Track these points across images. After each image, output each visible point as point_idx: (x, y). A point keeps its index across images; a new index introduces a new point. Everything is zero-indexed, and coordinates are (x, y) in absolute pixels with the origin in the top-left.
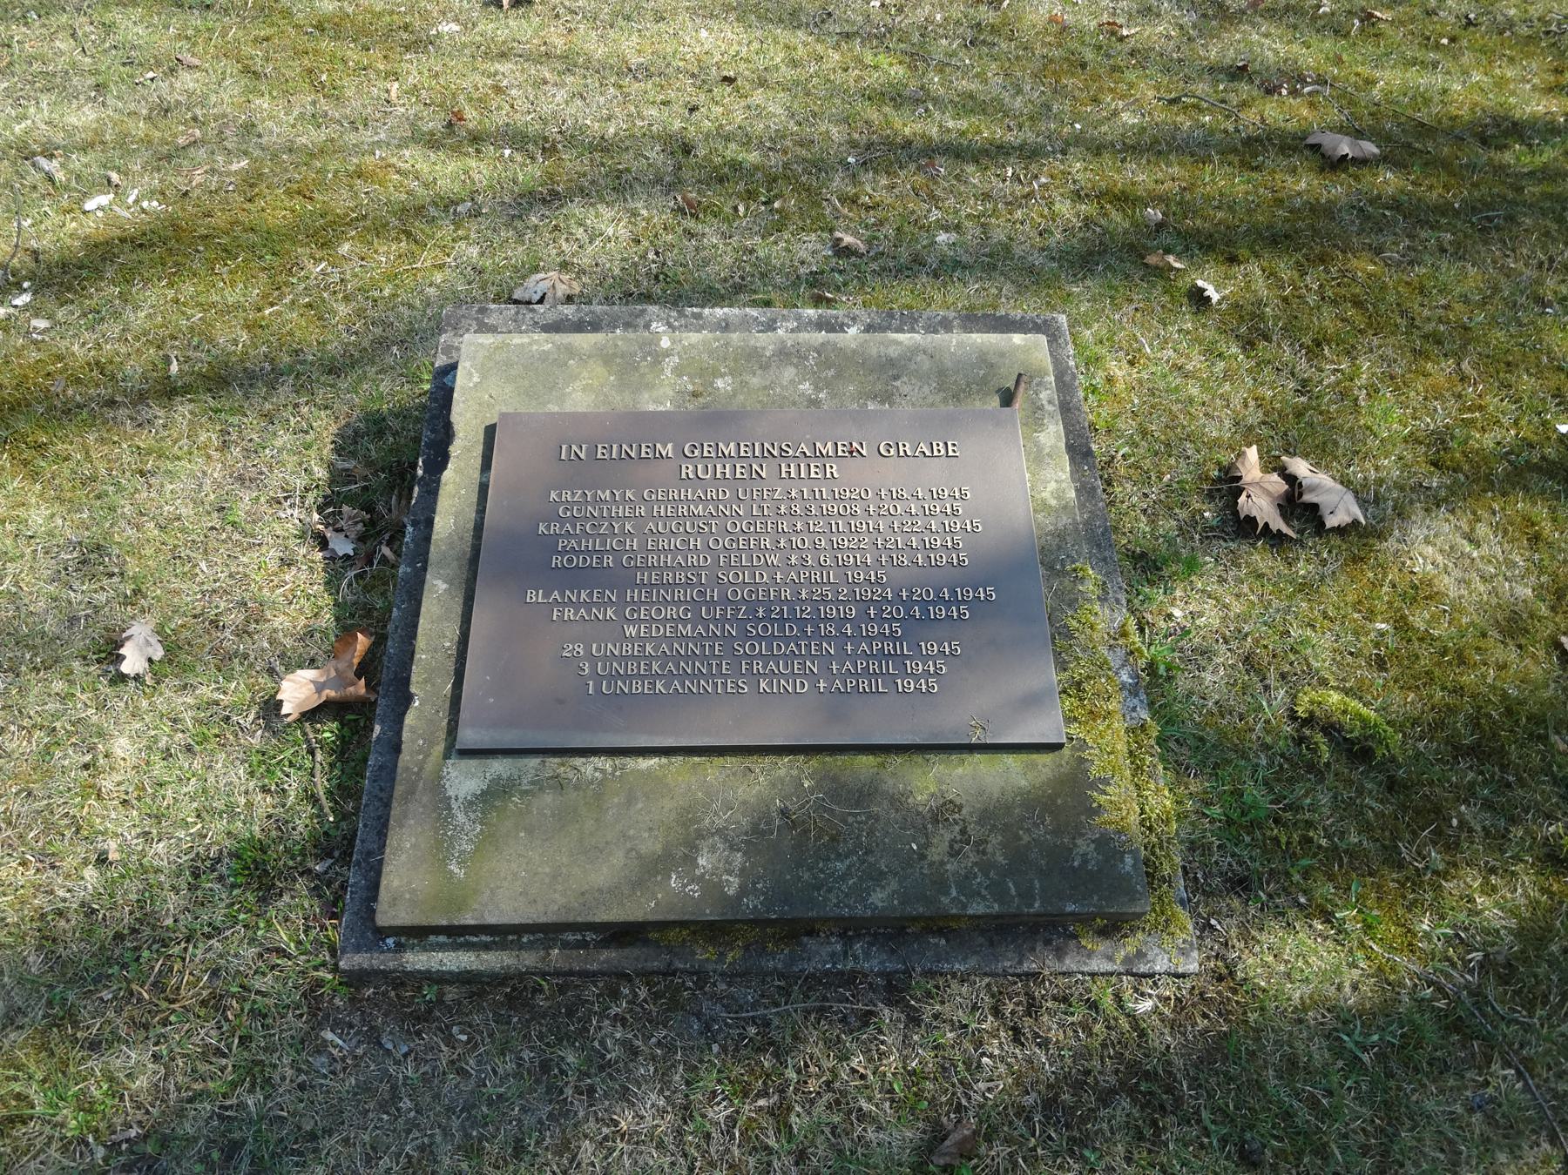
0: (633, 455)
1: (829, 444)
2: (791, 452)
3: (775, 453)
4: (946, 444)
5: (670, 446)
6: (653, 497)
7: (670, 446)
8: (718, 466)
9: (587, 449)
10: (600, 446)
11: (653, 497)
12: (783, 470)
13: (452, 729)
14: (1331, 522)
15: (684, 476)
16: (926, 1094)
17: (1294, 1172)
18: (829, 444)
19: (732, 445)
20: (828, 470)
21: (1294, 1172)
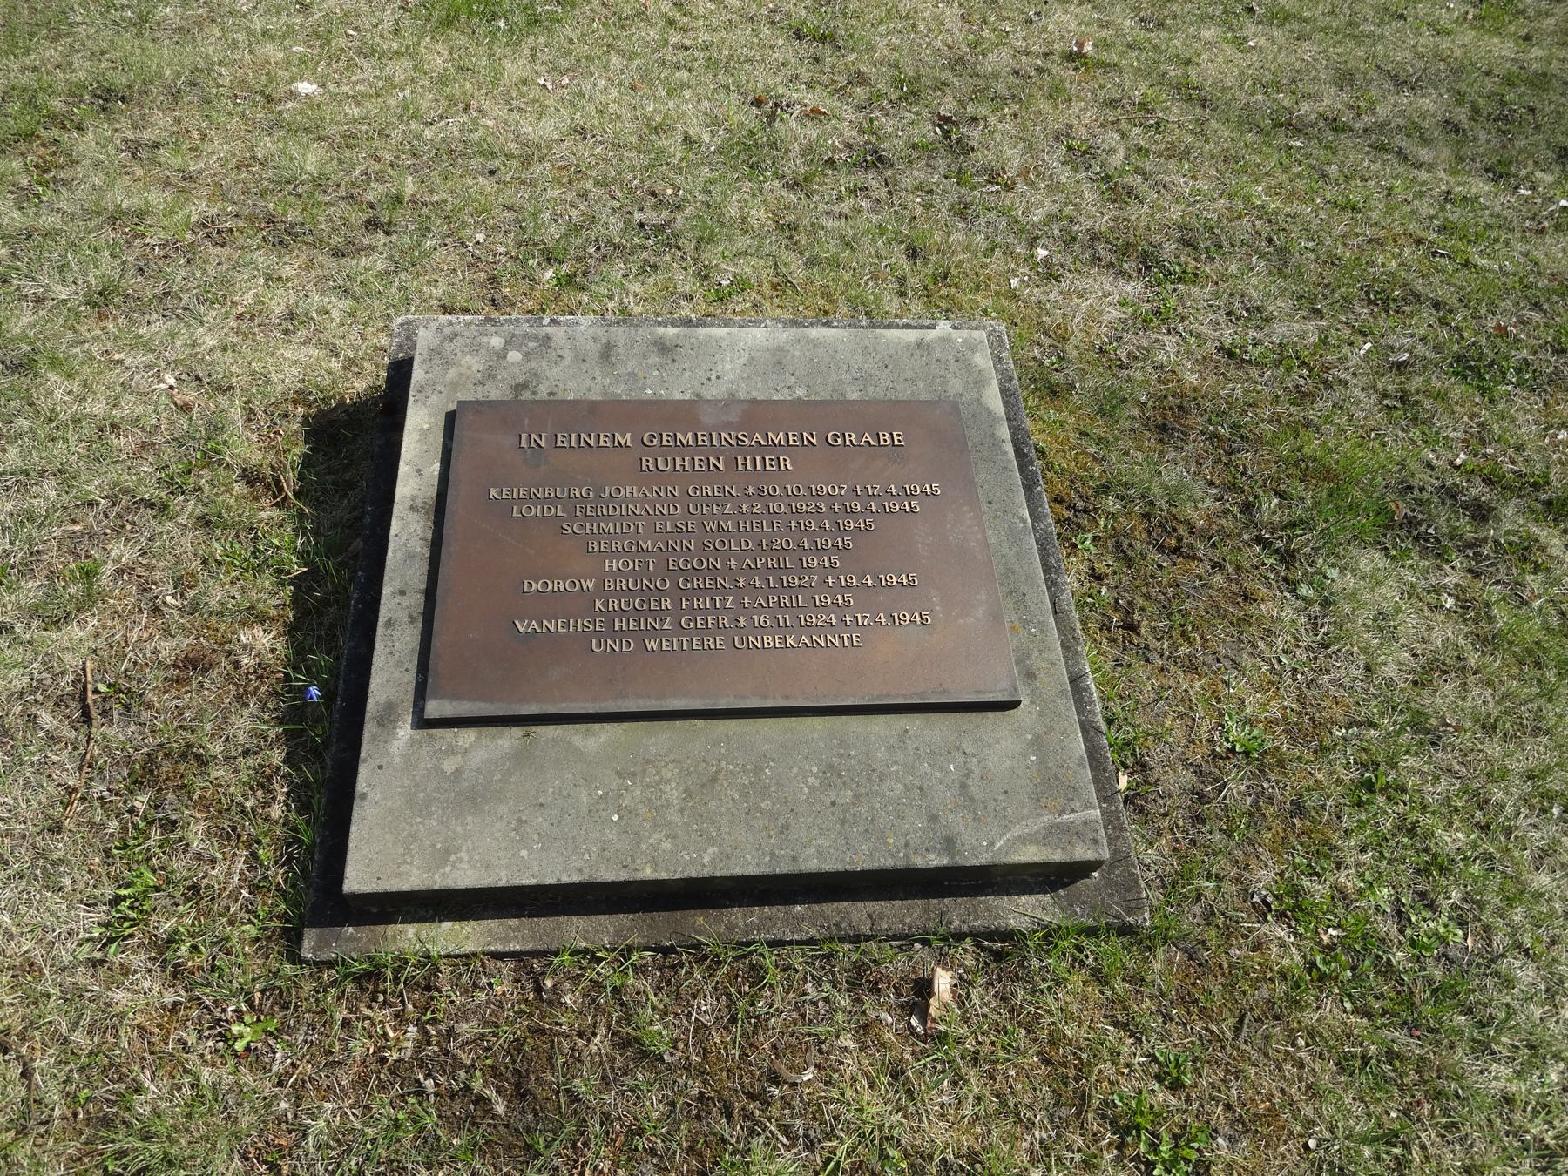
0: (592, 443)
1: (781, 435)
2: (747, 442)
3: (733, 442)
4: (891, 435)
5: (628, 435)
6: (689, 585)
7: (628, 435)
8: (678, 459)
9: (546, 438)
10: (559, 435)
11: (689, 585)
12: (740, 463)
13: (421, 693)
14: (968, 943)
15: (644, 468)
16: (407, 782)
17: (1562, 435)
18: (781, 435)
19: (690, 435)
20: (782, 463)
21: (1562, 435)
